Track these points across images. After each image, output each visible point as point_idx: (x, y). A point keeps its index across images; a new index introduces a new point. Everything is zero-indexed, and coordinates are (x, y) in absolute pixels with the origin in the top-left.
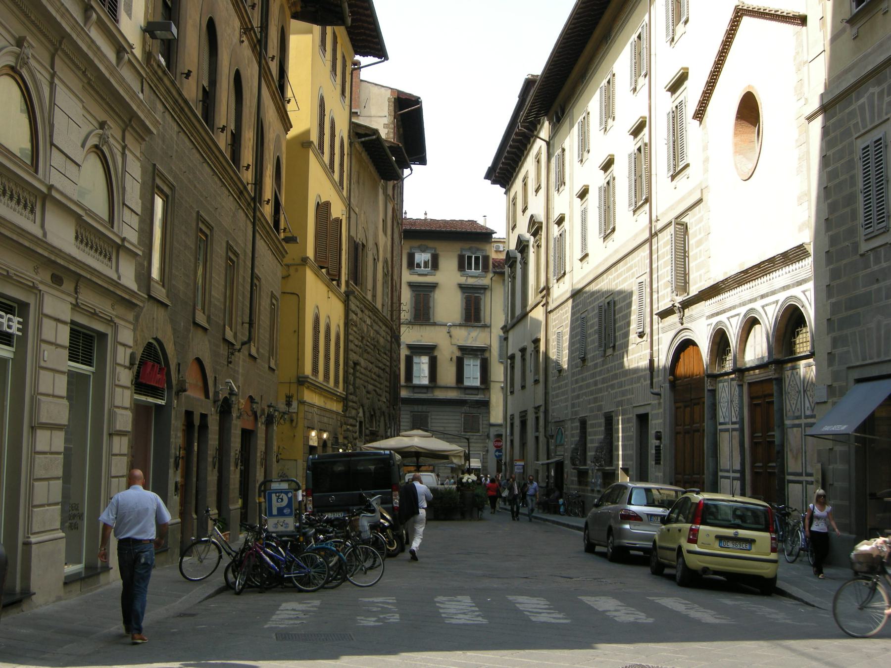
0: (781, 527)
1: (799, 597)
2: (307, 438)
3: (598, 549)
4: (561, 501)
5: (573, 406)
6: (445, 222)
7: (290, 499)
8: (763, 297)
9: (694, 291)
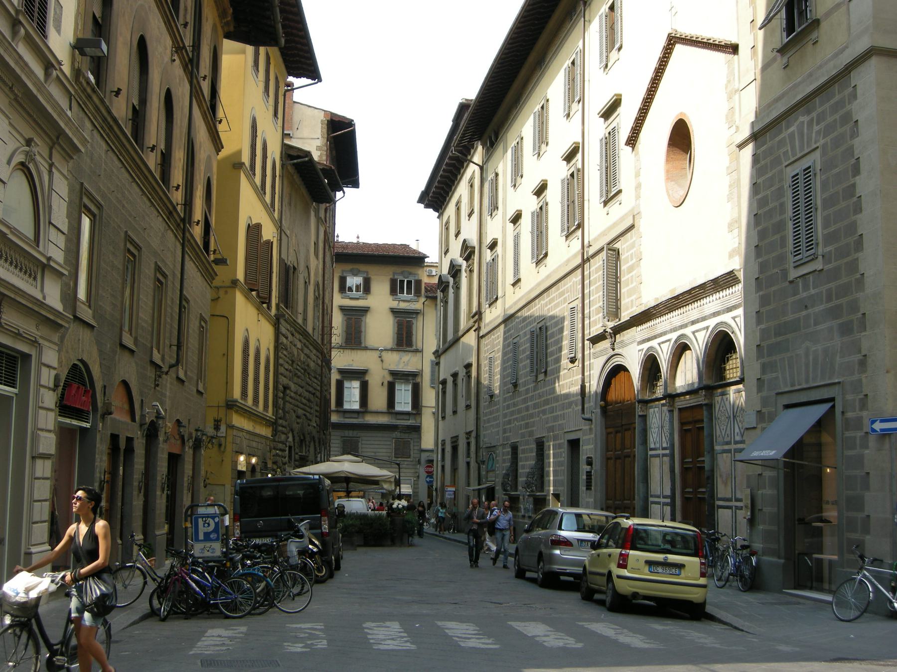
0: (711, 553)
2: (235, 463)
5: (505, 431)
7: (217, 524)
9: (625, 316)
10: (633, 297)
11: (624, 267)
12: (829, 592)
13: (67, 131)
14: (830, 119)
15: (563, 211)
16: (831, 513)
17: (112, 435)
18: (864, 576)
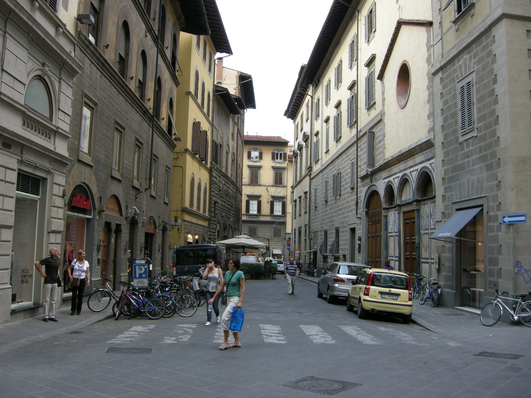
0: (418, 286)
1: (423, 325)
2: (187, 238)
3: (324, 296)
4: (315, 270)
5: (322, 224)
6: (266, 137)
7: (146, 269)
8: (410, 167)
9: (377, 165)
10: (381, 156)
11: (377, 141)
12: (479, 308)
13: (68, 60)
14: (480, 55)
15: (348, 115)
16: (480, 266)
17: (106, 223)
18: (498, 301)
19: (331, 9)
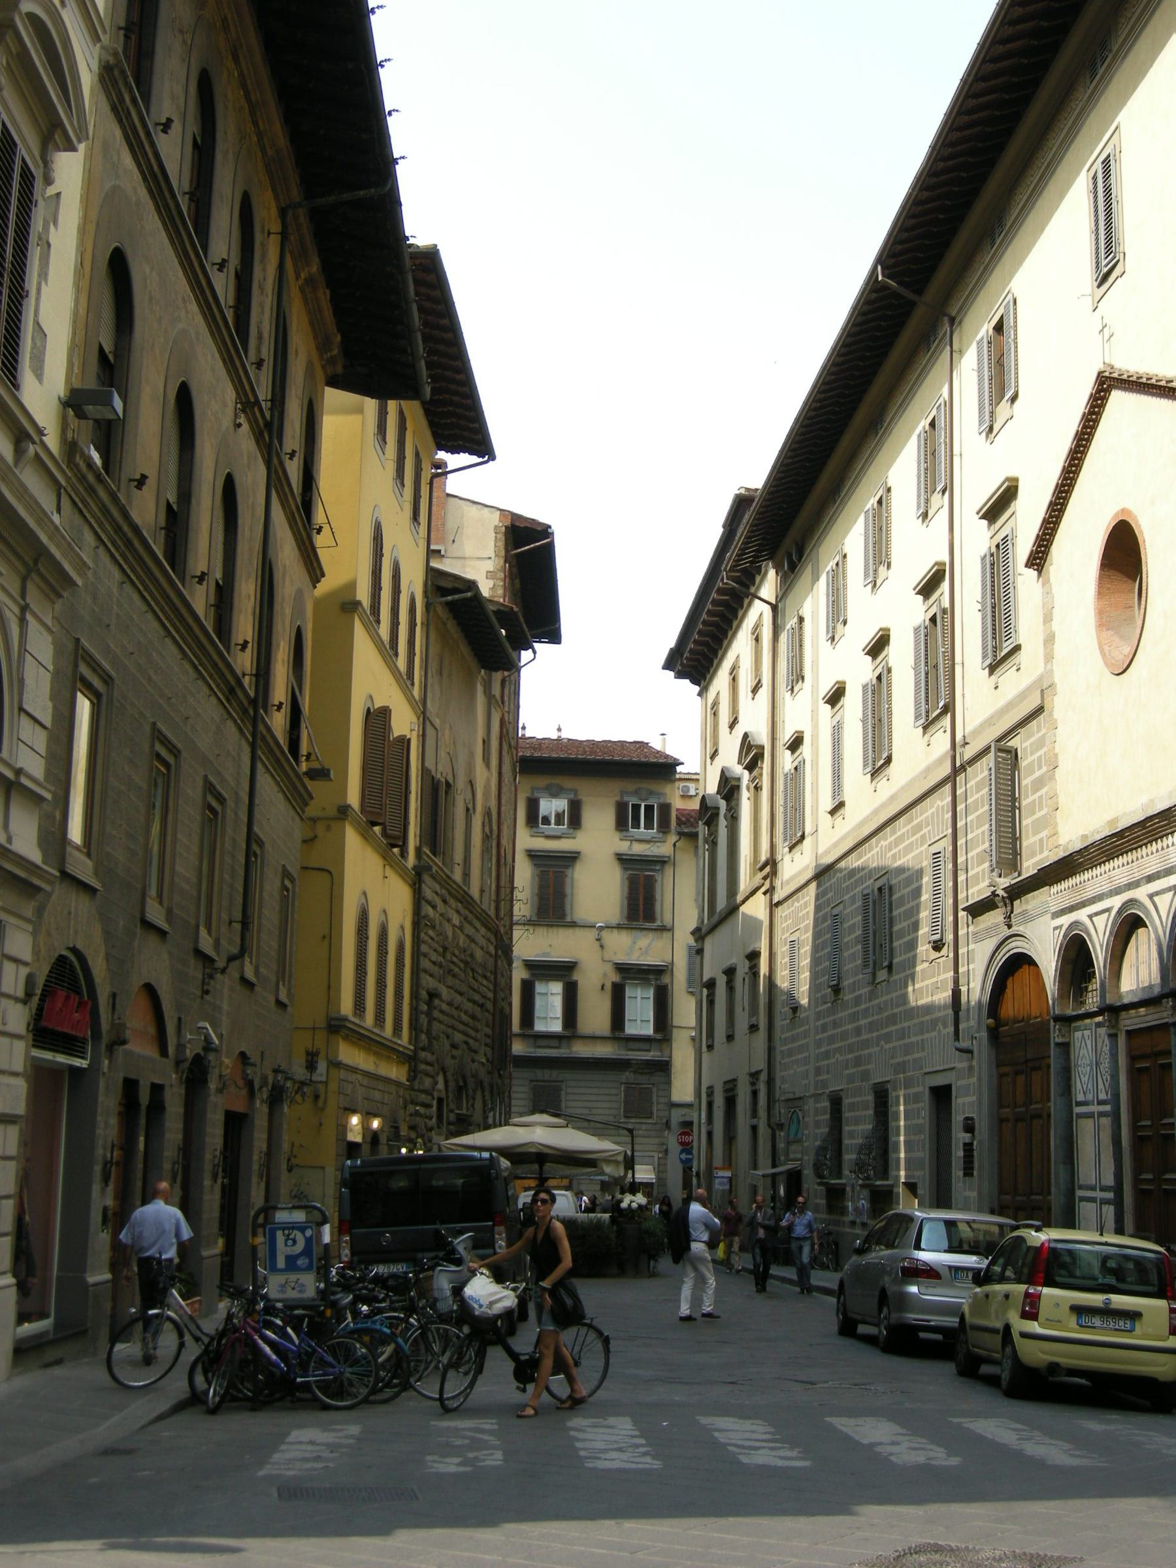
2: (343, 1128)
3: (862, 1329)
5: (818, 1071)
6: (593, 744)
7: (309, 1241)
8: (1150, 879)
9: (1030, 867)
10: (1044, 834)
13: (53, 549)
15: (917, 683)
19: (855, 308)
